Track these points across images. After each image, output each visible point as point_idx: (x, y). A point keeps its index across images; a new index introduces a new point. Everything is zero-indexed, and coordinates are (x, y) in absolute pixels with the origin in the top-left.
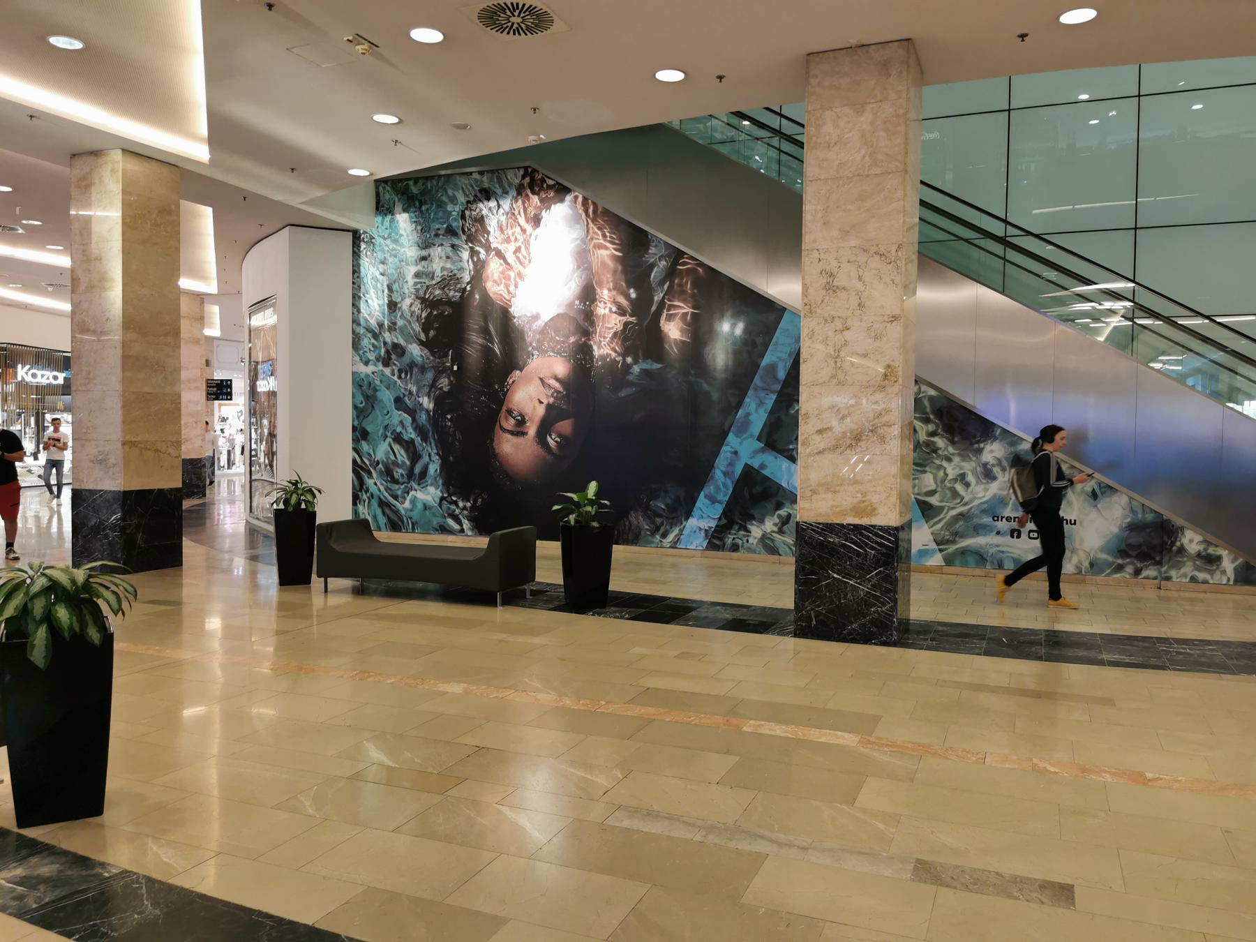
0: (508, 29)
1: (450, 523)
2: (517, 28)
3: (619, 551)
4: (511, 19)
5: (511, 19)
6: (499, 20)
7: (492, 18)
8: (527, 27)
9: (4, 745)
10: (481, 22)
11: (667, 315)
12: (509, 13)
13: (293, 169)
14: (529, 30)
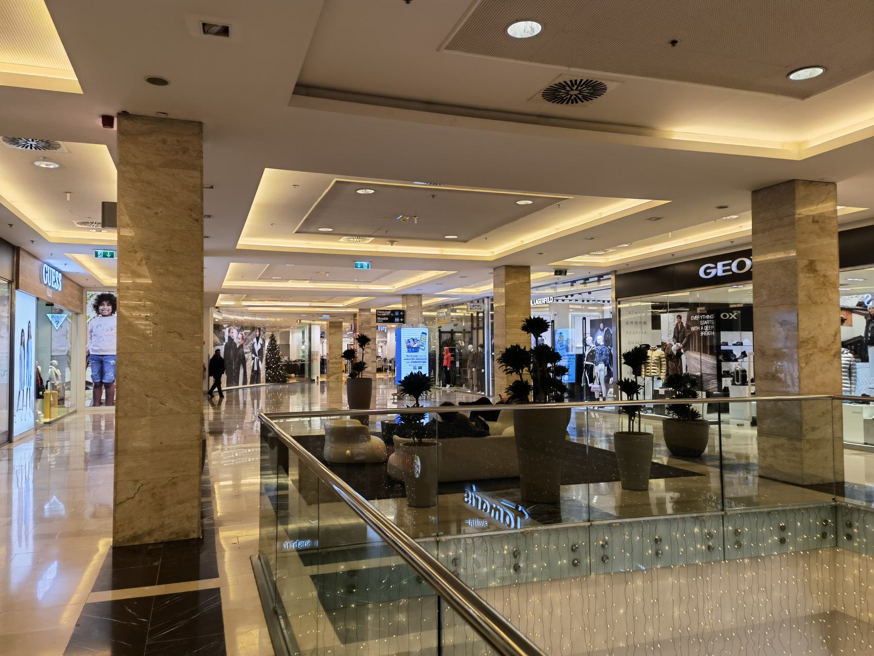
0: (567, 100)
1: (139, 281)
2: (573, 86)
3: (574, 381)
4: (569, 93)
5: (569, 93)
6: (559, 95)
7: (554, 94)
8: (583, 96)
9: (723, 350)
10: (544, 98)
11: (736, 507)
12: (568, 89)
13: (433, 196)
14: (586, 98)
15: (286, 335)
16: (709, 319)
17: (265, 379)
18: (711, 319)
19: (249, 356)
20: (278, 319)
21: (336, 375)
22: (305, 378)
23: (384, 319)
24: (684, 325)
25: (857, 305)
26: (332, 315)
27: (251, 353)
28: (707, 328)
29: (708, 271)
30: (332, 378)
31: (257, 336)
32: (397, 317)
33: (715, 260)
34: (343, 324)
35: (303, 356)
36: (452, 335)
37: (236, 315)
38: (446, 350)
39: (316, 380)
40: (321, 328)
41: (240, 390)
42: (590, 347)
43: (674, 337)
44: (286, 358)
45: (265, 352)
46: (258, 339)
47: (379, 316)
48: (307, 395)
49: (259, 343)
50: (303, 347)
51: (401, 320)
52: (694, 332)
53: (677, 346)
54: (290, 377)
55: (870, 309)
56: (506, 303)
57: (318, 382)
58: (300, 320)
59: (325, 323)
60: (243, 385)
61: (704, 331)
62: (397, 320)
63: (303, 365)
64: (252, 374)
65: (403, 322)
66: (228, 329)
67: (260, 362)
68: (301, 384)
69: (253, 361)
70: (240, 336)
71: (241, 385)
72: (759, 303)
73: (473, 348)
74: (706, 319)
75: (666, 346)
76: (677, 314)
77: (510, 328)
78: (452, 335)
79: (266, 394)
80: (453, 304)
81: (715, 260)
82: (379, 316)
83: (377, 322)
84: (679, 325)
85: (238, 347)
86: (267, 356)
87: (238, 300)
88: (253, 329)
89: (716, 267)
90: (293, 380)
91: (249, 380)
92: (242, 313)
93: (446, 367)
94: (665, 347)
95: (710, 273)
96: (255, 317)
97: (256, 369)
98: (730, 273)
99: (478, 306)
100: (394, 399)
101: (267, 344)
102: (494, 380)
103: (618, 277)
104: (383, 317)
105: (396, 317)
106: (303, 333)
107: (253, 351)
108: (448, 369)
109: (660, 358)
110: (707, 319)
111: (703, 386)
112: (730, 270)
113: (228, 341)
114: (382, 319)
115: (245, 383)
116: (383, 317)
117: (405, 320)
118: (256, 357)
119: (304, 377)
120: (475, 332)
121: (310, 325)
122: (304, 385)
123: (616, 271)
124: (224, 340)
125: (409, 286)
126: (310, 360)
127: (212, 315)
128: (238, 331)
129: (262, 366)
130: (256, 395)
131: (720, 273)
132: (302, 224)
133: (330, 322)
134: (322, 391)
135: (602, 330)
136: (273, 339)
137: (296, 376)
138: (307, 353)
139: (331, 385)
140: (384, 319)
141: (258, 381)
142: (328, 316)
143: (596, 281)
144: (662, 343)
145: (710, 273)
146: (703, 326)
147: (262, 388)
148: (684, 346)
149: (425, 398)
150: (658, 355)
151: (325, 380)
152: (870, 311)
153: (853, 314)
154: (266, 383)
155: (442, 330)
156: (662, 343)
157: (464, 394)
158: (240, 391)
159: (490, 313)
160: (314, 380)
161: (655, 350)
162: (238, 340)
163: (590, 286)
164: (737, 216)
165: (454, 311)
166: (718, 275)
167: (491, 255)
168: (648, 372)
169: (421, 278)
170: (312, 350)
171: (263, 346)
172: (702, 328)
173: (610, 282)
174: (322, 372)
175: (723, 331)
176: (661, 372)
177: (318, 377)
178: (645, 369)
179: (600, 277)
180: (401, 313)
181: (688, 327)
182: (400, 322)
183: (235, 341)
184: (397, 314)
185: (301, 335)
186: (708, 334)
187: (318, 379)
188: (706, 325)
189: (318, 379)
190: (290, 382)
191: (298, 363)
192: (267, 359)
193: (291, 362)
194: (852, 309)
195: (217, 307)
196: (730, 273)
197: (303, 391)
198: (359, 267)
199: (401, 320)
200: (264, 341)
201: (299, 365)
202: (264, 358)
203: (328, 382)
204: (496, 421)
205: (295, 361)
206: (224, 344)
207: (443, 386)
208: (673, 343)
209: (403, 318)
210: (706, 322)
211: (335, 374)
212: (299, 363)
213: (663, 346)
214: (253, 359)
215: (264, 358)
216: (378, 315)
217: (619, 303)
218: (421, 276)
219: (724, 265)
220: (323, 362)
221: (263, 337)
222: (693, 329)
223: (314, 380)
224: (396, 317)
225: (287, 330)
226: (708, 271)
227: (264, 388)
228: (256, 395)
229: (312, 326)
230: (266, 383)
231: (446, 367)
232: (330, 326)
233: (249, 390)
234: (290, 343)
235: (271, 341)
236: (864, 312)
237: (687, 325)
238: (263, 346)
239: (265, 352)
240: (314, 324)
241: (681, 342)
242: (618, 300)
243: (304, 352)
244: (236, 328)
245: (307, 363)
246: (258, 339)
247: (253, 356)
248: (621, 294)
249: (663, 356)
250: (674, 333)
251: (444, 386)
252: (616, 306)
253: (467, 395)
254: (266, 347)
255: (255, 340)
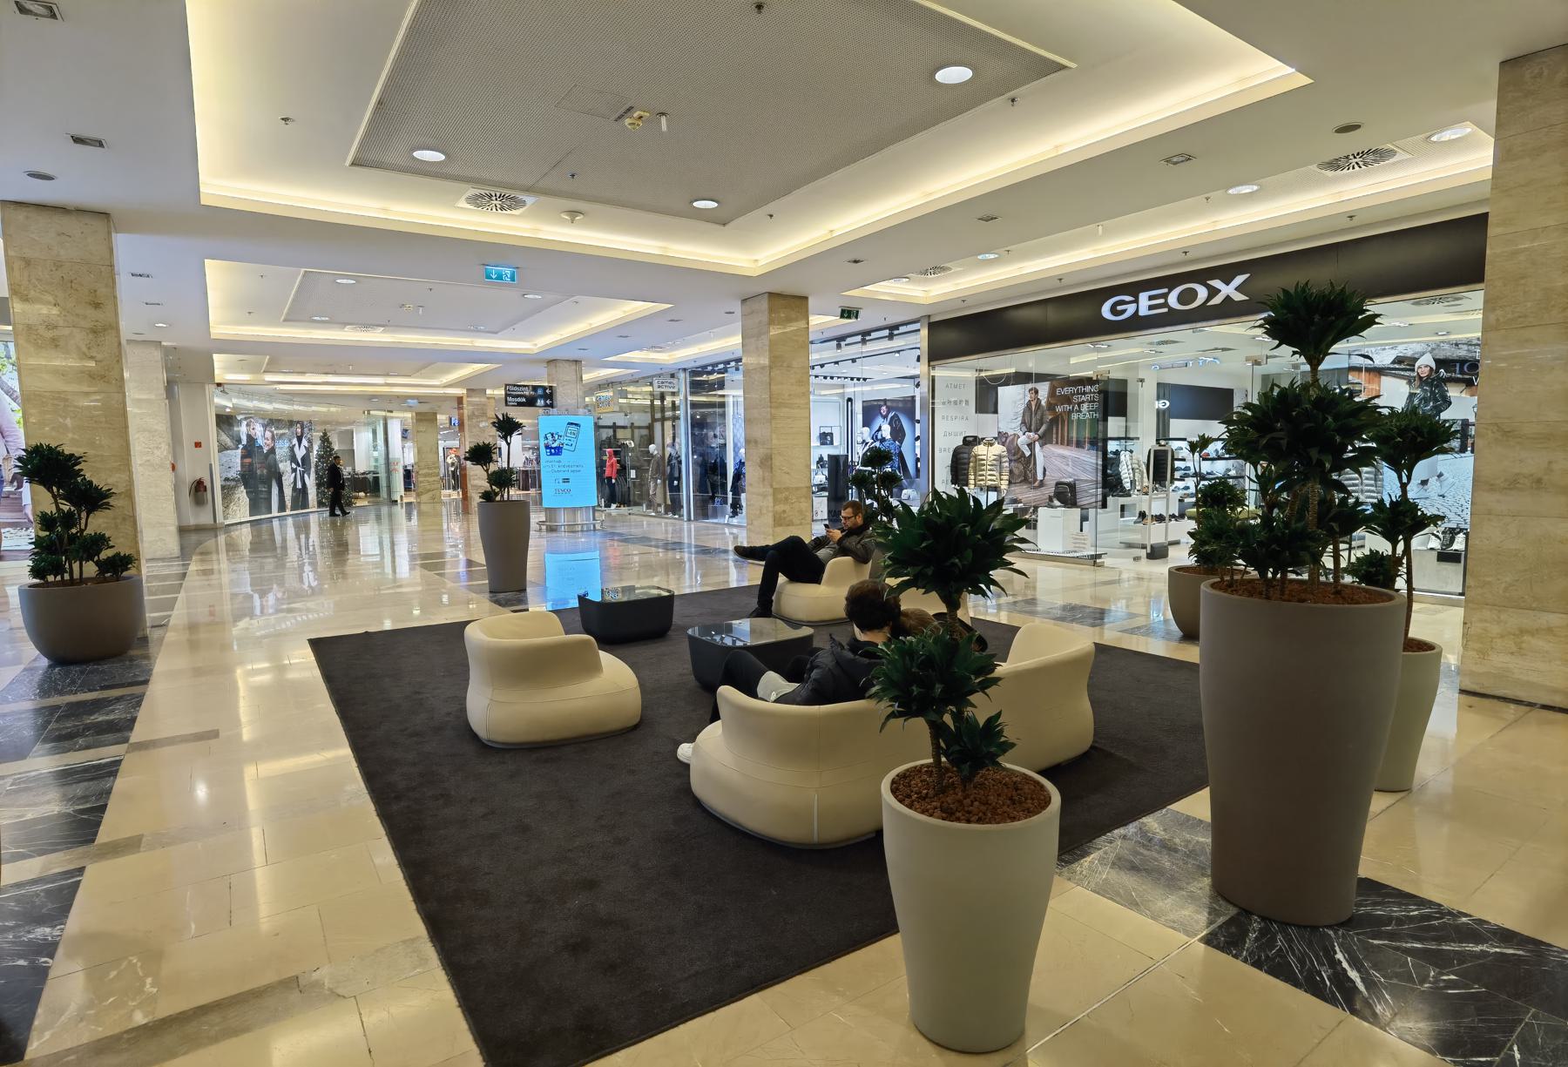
15: (349, 437)
16: (1091, 392)
17: (315, 501)
18: (1094, 393)
19: (285, 466)
20: (333, 409)
21: (431, 493)
22: (381, 499)
23: (519, 400)
24: (1043, 403)
25: (1393, 362)
26: (422, 399)
27: (289, 462)
28: (1085, 407)
29: (1119, 308)
30: (425, 498)
31: (299, 435)
32: (541, 397)
33: (1134, 289)
34: (438, 417)
35: (376, 467)
36: (615, 432)
37: (259, 400)
38: (609, 452)
39: (399, 501)
40: (402, 423)
41: (273, 520)
42: (867, 443)
43: (1023, 422)
44: (349, 469)
45: (314, 459)
46: (300, 440)
47: (510, 395)
48: (385, 527)
49: (302, 445)
50: (376, 454)
51: (548, 402)
52: (1061, 414)
53: (1029, 437)
54: (357, 498)
55: (1419, 367)
56: (771, 361)
57: (402, 504)
58: (369, 411)
59: (409, 415)
60: (250, 516)
61: (1081, 412)
62: (540, 402)
63: (376, 480)
64: (294, 494)
65: (552, 406)
66: (245, 423)
67: (306, 476)
68: (375, 507)
69: (294, 474)
70: (268, 434)
71: (275, 513)
72: (1501, 319)
73: (657, 449)
74: (1084, 393)
75: (1007, 438)
76: (1030, 386)
77: (777, 407)
78: (615, 432)
79: (320, 525)
80: (620, 383)
81: (1134, 289)
82: (510, 395)
83: (507, 405)
84: (1033, 404)
85: (265, 452)
86: (317, 466)
87: (255, 369)
88: (291, 423)
89: (1136, 301)
90: (362, 500)
91: (288, 503)
92: (270, 397)
93: (610, 479)
94: (1004, 440)
95: (1124, 311)
96: (293, 405)
97: (299, 485)
98: (1165, 310)
99: (670, 383)
100: (540, 530)
101: (316, 447)
102: (541, 493)
103: (933, 327)
104: (517, 396)
105: (542, 397)
106: (374, 432)
107: (293, 458)
108: (614, 481)
109: (1000, 457)
110: (1087, 393)
111: (1075, 498)
112: (1166, 305)
113: (247, 442)
114: (516, 400)
115: (282, 507)
116: (517, 396)
117: (555, 402)
118: (298, 468)
119: (379, 496)
120: (658, 426)
121: (385, 420)
122: (380, 509)
123: (929, 316)
124: (239, 441)
125: (576, 338)
126: (389, 472)
127: (211, 401)
128: (265, 426)
129: (311, 482)
130: (302, 528)
131: (1143, 312)
132: (372, 121)
133: (416, 414)
134: (409, 518)
135: (885, 417)
136: (325, 439)
137: (366, 496)
138: (382, 461)
139: (424, 508)
140: (519, 400)
141: (305, 505)
142: (416, 401)
143: (886, 337)
144: (999, 433)
145: (1124, 311)
146: (1079, 404)
147: (311, 516)
148: (1040, 437)
149: (592, 528)
150: (997, 453)
151: (412, 499)
152: (1420, 371)
153: (1383, 378)
154: (319, 507)
155: (601, 423)
156: (999, 433)
157: (644, 518)
158: (276, 523)
159: (690, 398)
160: (396, 501)
161: (991, 445)
162: (266, 441)
163: (849, 351)
164: (1255, 188)
165: (624, 395)
166: (1141, 313)
167: (752, 265)
168: (983, 480)
169: (591, 324)
170: (390, 456)
171: (309, 450)
172: (1076, 407)
173: (922, 338)
174: (407, 488)
175: (1112, 415)
176: (1001, 480)
177: (401, 497)
178: (975, 475)
179: (893, 330)
180: (548, 391)
181: (1051, 407)
182: (546, 405)
183: (260, 442)
184: (540, 392)
185: (371, 435)
186: (1088, 416)
187: (402, 500)
188: (1083, 402)
189: (402, 500)
190: (357, 505)
191: (368, 476)
192: (317, 473)
193: (357, 474)
194: (1383, 369)
195: (219, 385)
196: (1165, 310)
197: (378, 518)
198: (494, 277)
199: (548, 402)
200: (310, 441)
201: (371, 480)
202: (313, 470)
203: (419, 503)
204: (820, 584)
205: (363, 474)
206: (241, 446)
207: (605, 506)
208: (1020, 433)
209: (552, 400)
210: (1083, 398)
211: (429, 491)
212: (370, 477)
213: (1002, 438)
214: (294, 470)
215: (313, 470)
216: (508, 393)
217: (934, 368)
218: (591, 322)
219: (1151, 298)
220: (408, 475)
221: (309, 436)
222: (1059, 409)
223: (396, 501)
224: (542, 397)
225: (349, 428)
226: (1119, 308)
227: (316, 515)
228: (302, 528)
229: (389, 422)
230: (319, 507)
231: (610, 479)
232: (418, 420)
233: (290, 521)
234: (355, 448)
235: (323, 442)
236: (1407, 373)
237: (1049, 403)
238: (309, 450)
239: (314, 459)
240: (392, 418)
241: (1036, 431)
242: (932, 363)
243: (376, 460)
244: (261, 421)
245: (382, 476)
246: (300, 440)
247: (294, 466)
248: (937, 354)
249: (1005, 453)
250: (1023, 416)
251: (608, 506)
252: (929, 373)
253: (648, 519)
254: (315, 452)
255: (295, 441)
